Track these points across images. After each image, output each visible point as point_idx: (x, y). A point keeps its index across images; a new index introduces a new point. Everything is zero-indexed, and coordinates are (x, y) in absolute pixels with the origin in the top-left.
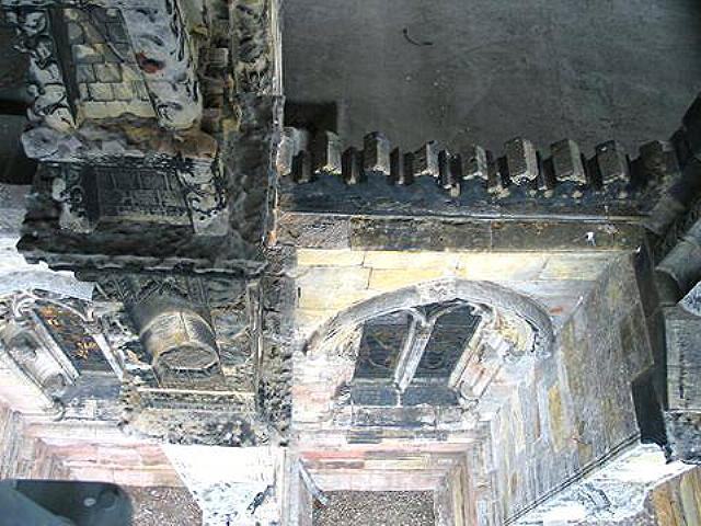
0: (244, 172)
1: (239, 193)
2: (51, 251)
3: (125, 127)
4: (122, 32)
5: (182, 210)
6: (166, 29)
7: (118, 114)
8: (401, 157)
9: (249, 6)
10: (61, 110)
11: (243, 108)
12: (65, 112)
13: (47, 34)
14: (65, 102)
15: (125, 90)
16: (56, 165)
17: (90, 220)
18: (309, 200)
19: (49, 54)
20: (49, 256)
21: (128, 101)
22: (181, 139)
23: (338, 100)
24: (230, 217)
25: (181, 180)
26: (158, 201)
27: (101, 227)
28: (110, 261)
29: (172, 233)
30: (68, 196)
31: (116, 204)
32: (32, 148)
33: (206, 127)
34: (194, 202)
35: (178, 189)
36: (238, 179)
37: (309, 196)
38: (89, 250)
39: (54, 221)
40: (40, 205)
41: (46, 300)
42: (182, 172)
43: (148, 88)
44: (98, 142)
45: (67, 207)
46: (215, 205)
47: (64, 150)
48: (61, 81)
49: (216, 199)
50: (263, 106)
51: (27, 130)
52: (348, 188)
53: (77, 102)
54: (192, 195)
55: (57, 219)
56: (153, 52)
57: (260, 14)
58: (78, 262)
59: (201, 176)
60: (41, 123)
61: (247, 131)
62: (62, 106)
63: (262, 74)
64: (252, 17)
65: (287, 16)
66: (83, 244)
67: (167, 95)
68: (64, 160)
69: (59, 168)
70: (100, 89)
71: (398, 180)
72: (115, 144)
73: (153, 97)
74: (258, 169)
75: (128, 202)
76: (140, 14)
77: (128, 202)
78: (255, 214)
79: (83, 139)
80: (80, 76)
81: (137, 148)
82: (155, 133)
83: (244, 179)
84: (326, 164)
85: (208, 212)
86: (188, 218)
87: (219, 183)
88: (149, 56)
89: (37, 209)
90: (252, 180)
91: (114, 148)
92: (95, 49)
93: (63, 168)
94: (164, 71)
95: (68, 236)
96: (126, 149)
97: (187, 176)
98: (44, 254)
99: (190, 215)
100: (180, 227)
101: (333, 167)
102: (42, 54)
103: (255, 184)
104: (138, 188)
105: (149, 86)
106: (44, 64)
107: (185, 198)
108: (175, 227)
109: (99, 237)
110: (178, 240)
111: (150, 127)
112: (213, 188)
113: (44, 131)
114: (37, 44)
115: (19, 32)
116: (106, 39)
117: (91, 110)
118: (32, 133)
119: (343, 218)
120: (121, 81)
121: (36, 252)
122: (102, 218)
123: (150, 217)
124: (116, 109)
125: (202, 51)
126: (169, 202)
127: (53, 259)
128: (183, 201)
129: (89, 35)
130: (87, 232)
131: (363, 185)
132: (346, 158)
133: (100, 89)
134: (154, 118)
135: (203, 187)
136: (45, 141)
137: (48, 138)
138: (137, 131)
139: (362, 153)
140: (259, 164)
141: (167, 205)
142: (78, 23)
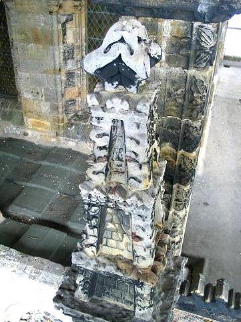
0: (163, 291)
1: (159, 301)
2: (68, 306)
3: (117, 261)
4: (128, 222)
5: (131, 303)
6: (148, 225)
7: (116, 254)
8: (234, 294)
9: (178, 213)
10: (92, 247)
11: (168, 260)
12: (94, 249)
13: (98, 216)
14: (95, 244)
15: (122, 245)
16: (82, 269)
17: (89, 296)
18: (186, 305)
19: (96, 224)
20: (65, 308)
21: (122, 250)
22: (142, 273)
23: (205, 258)
24: (153, 311)
25: (136, 290)
26: (121, 296)
27: (92, 301)
28: (93, 319)
29: (124, 313)
30: (83, 283)
31: (102, 292)
32: (75, 260)
33: (154, 269)
34: (139, 301)
35: (133, 293)
36: (160, 294)
37: (185, 303)
38: (84, 310)
39: (72, 292)
40: (68, 282)
41: (48, 317)
42: (137, 286)
43: (133, 247)
44: (104, 265)
45: (80, 288)
46: (148, 305)
47: (89, 264)
48: (97, 235)
49: (149, 303)
50: (177, 261)
51: (75, 251)
52: (206, 304)
53: (100, 245)
54: (139, 298)
55: (74, 291)
56: (140, 233)
57: (182, 218)
58: (77, 315)
59: (146, 291)
60: (82, 250)
61: (168, 271)
62: (94, 246)
63: (177, 243)
64: (178, 218)
65: (74, 15)
66: (82, 307)
67: (140, 252)
68: (87, 268)
69: (83, 271)
70: (111, 242)
71: (231, 305)
72: (112, 268)
73: (134, 252)
74: (170, 291)
75: (108, 293)
76: (139, 217)
77: (108, 293)
78: (165, 314)
79: (98, 262)
80: (105, 235)
81: (121, 272)
82: (131, 267)
83: (163, 294)
84: (197, 289)
85: (144, 308)
86: (133, 308)
87: (152, 295)
88: (137, 234)
89: (66, 284)
90: (167, 296)
91: (111, 269)
92: (115, 226)
93: (84, 271)
94: (142, 242)
95: (77, 302)
96: (116, 271)
97: (139, 290)
98: (63, 306)
99: (135, 307)
100: (129, 310)
101: (200, 292)
102: (93, 223)
103: (168, 298)
104: (115, 288)
105: (134, 246)
106: (93, 227)
107: (135, 298)
108: (126, 310)
109: (91, 306)
110: (126, 317)
111: (129, 264)
112: (149, 297)
113: (82, 254)
114: (92, 219)
115: (86, 213)
116: (121, 223)
117: (105, 250)
118: (77, 253)
119: (200, 318)
120: (122, 241)
121: (61, 305)
122: (95, 297)
123: (116, 302)
124: (116, 252)
125: (158, 234)
126: (127, 298)
127: (67, 310)
128: (133, 299)
129: (114, 220)
130: (86, 301)
131: (213, 304)
132: (207, 288)
133: (111, 242)
134: (132, 260)
135: (145, 296)
136: (82, 258)
137: (83, 257)
138: (123, 264)
139: (215, 287)
140: (170, 289)
141: (126, 299)
142: (111, 215)
